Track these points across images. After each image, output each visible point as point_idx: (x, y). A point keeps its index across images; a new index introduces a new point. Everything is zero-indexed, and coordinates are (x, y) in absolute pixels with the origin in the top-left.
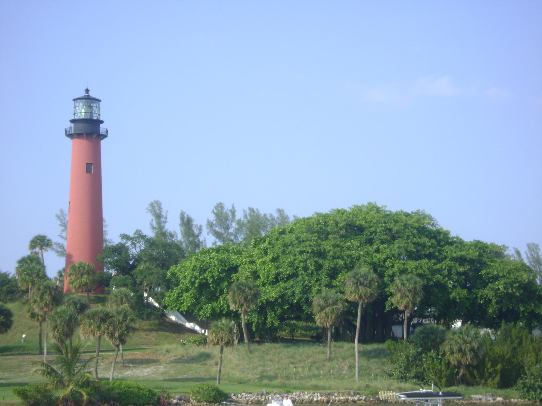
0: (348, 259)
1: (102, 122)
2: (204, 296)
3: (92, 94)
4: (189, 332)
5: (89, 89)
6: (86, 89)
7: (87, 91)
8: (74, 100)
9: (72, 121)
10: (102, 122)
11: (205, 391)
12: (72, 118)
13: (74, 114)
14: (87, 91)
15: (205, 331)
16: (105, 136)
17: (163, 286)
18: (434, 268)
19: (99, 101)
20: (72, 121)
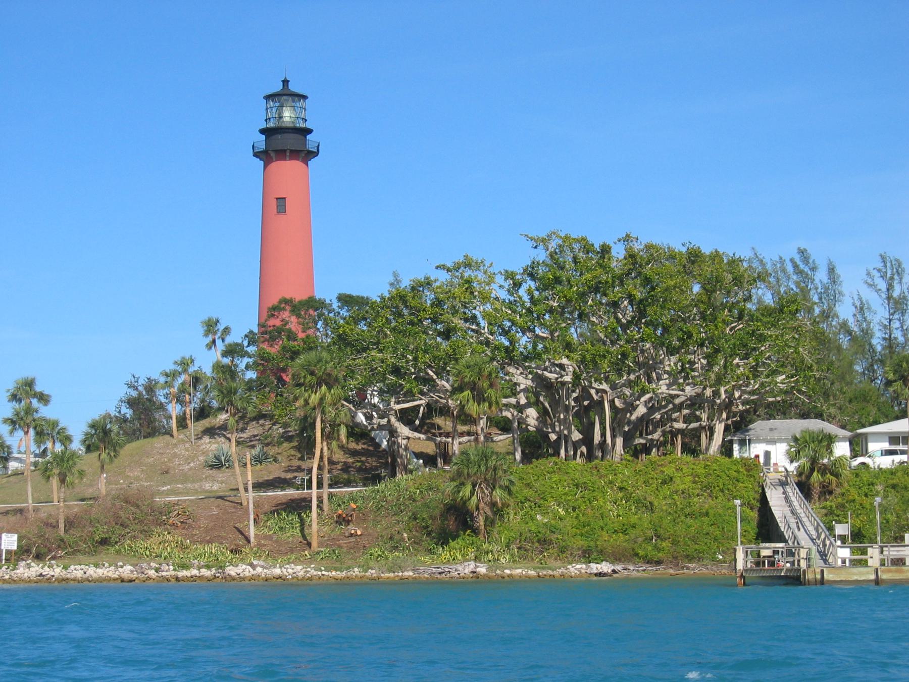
0: (799, 320)
1: (309, 131)
2: (818, 315)
3: (293, 87)
4: (849, 326)
5: (288, 79)
6: (283, 79)
7: (285, 82)
8: (268, 97)
9: (262, 131)
10: (309, 131)
11: (41, 435)
12: (264, 126)
13: (266, 120)
14: (285, 82)
15: (618, 344)
16: (316, 154)
17: (749, 305)
18: (41, 451)
19: (304, 97)
20: (262, 131)
